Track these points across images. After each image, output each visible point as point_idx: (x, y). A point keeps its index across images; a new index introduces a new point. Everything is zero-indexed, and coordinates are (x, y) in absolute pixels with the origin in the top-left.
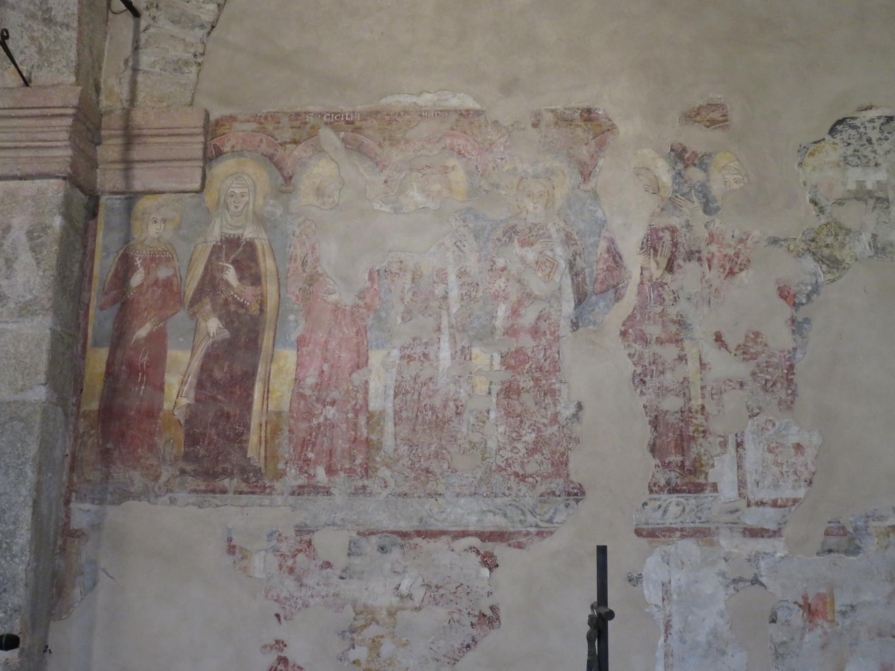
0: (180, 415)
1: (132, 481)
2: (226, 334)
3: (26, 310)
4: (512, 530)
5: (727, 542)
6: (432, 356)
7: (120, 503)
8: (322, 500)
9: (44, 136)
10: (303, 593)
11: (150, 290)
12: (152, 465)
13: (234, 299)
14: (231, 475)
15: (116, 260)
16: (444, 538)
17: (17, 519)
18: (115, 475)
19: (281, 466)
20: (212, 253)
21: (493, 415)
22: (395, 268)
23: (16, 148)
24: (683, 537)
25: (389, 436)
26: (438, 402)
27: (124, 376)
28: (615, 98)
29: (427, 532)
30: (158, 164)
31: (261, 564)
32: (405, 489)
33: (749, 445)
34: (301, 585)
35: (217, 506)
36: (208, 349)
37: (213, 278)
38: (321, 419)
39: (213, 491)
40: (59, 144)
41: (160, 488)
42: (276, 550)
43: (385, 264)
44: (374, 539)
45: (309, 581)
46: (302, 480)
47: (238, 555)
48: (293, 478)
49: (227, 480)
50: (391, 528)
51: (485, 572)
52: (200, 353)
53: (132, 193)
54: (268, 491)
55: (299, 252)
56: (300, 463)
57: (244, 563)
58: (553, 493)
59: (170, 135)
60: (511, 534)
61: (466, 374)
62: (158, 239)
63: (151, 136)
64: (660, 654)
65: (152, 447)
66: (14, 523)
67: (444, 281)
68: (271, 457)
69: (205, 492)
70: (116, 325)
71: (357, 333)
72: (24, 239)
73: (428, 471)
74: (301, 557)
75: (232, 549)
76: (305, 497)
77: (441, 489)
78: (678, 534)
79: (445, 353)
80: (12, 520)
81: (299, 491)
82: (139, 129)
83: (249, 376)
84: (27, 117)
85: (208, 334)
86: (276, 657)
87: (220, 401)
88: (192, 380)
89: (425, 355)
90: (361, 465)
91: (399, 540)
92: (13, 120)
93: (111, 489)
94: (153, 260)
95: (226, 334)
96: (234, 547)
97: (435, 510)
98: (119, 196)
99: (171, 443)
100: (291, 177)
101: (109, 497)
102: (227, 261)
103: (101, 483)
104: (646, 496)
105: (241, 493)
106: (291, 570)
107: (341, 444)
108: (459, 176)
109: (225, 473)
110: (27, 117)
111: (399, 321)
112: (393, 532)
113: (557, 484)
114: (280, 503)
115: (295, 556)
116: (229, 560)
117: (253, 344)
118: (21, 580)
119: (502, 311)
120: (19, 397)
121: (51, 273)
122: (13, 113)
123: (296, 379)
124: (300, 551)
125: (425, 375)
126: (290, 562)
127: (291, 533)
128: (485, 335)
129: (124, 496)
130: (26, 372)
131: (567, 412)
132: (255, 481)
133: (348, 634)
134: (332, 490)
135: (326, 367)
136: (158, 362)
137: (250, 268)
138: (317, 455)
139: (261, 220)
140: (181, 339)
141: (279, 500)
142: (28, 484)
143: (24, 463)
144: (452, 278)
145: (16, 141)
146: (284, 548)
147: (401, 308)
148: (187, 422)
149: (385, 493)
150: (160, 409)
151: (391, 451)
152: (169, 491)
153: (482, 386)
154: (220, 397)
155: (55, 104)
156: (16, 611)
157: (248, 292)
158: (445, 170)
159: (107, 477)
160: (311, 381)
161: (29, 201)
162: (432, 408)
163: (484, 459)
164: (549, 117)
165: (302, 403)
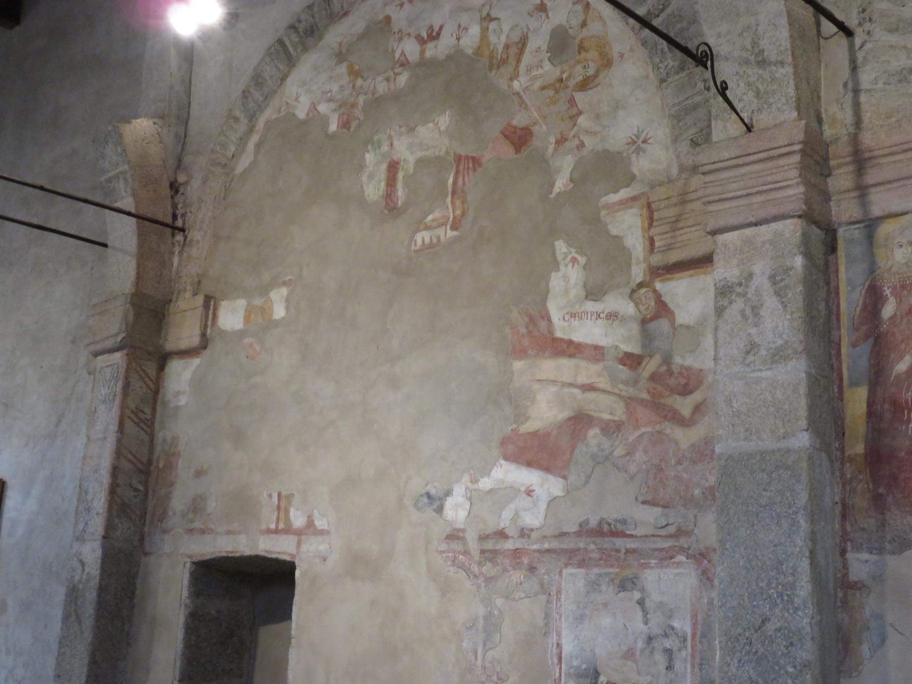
3: (778, 356)
9: (775, 178)
15: (863, 292)
23: (748, 195)
27: (888, 416)
30: (895, 185)
40: (790, 183)
53: (871, 219)
63: (884, 156)
66: (793, 574)
70: (872, 362)
93: (889, 537)
98: (857, 226)
103: (877, 531)
110: (755, 162)
118: (807, 633)
120: (783, 444)
121: (799, 314)
122: (740, 161)
156: (805, 666)
159: (883, 525)
161: (767, 246)
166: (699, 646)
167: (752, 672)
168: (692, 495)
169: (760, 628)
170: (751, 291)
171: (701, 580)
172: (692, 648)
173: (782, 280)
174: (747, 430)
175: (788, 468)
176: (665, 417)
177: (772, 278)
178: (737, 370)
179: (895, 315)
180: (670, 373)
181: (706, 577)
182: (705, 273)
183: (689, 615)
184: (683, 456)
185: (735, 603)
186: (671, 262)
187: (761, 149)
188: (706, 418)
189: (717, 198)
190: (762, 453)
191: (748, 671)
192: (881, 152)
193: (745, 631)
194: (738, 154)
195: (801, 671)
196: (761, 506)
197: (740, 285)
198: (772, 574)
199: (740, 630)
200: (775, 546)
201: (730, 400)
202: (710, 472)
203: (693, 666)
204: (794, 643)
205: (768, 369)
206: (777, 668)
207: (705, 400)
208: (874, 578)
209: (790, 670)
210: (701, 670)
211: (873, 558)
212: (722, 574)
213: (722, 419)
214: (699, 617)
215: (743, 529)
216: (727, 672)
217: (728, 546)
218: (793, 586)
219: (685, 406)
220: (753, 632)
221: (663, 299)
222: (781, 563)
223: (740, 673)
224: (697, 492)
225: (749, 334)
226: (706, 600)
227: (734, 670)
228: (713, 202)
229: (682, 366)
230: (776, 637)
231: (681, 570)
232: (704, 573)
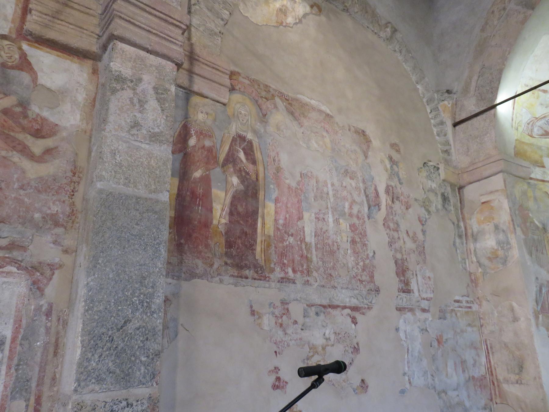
0: (222, 229)
1: (197, 266)
2: (242, 187)
3: (154, 138)
4: (360, 306)
5: (418, 313)
6: (326, 219)
7: (189, 280)
8: (292, 286)
9: (170, 33)
10: (287, 338)
11: (200, 151)
12: (209, 257)
13: (244, 169)
14: (249, 268)
15: (180, 126)
16: (339, 309)
17: (155, 284)
18: (186, 261)
19: (272, 266)
20: (233, 140)
21: (349, 252)
22: (309, 174)
23: (149, 31)
24: (408, 311)
25: (314, 256)
26: (330, 242)
27: (188, 199)
28: (371, 130)
29: (332, 305)
30: (206, 80)
31: (267, 322)
32: (323, 283)
33: (418, 276)
34: (286, 334)
35: (244, 286)
36: (234, 193)
37: (233, 155)
38: (288, 243)
39: (241, 277)
40: (177, 42)
41: (213, 272)
42: (273, 313)
43: (306, 171)
44: (313, 308)
45: (289, 331)
46: (282, 275)
47: (256, 316)
48: (278, 274)
49: (247, 271)
50: (319, 303)
51: (353, 325)
52: (230, 195)
53: (190, 90)
54: (267, 279)
55: (273, 154)
56: (281, 265)
57: (259, 321)
58: (371, 290)
59: (213, 68)
60: (360, 308)
61: (339, 232)
62: (204, 123)
63: (203, 63)
64: (406, 362)
65: (207, 246)
66: (153, 287)
67: (327, 186)
68: (268, 260)
69: (237, 277)
70: (182, 166)
71: (298, 202)
72: (151, 92)
73: (331, 275)
74: (284, 317)
75: (253, 313)
76: (284, 284)
77: (336, 285)
78: (407, 310)
79: (331, 220)
80: (151, 285)
81: (282, 280)
82: (198, 57)
83: (255, 213)
84: (155, 16)
85: (233, 185)
86: (275, 377)
87: (242, 224)
88: (227, 209)
89: (324, 219)
90: (306, 269)
91: (323, 309)
92: (145, 13)
93: (184, 269)
94: (201, 134)
95: (242, 187)
96: (254, 311)
97: (335, 295)
98: (181, 90)
99: (218, 244)
100: (265, 115)
101: (183, 275)
102: (240, 147)
103: (178, 265)
104: (397, 293)
105: (255, 279)
106: (281, 325)
107: (297, 258)
108: (327, 140)
109: (248, 267)
110: (155, 16)
111: (313, 200)
112: (320, 305)
113: (371, 286)
114: (273, 287)
115: (282, 317)
116: (252, 319)
117: (255, 195)
118: (159, 330)
119: (347, 205)
120: (153, 196)
121: (172, 119)
122: (148, 9)
123: (275, 220)
124: (284, 314)
125: (325, 228)
126: (280, 321)
127: (278, 304)
128: (343, 214)
129: (192, 275)
130: (157, 180)
131: (371, 254)
132: (261, 273)
133: (306, 361)
134: (296, 281)
135: (287, 216)
136: (207, 194)
137: (250, 155)
138: (288, 261)
139: (255, 132)
140: (219, 184)
141: (273, 284)
142: (162, 259)
143: (159, 244)
144: (329, 186)
145: (150, 27)
146: (277, 313)
147: (313, 195)
148: (226, 233)
149: (316, 284)
150: (211, 223)
151: (316, 263)
152: (219, 274)
153: (345, 239)
154: (241, 222)
155: (176, 17)
156: (156, 355)
157: (250, 168)
158: (323, 137)
159: (181, 262)
160: (281, 222)
161: (154, 69)
162: (329, 245)
163: (349, 272)
164: (353, 129)
165: (279, 233)
166: (19, 348)
167: (110, 364)
168: (32, 217)
169: (122, 327)
170: (139, 89)
171: (31, 290)
172: (10, 350)
173: (162, 94)
174: (126, 179)
175: (156, 213)
176: (14, 147)
177: (155, 89)
178: (123, 135)
179: (195, 146)
180: (26, 117)
181: (37, 288)
182: (71, 61)
183: (12, 321)
184: (29, 183)
185: (101, 308)
186: (47, 37)
187: (163, 12)
188: (57, 161)
189: (128, 19)
190: (137, 198)
191: (108, 364)
192: (203, 61)
193: (109, 330)
194: (148, 3)
195: (153, 359)
196: (132, 235)
197: (132, 81)
198: (137, 286)
199: (104, 330)
200: (141, 265)
201: (115, 154)
202: (54, 203)
203: (9, 367)
204: (149, 338)
205: (147, 144)
206: (133, 359)
207: (56, 148)
208: (173, 294)
209: (143, 359)
210: (16, 370)
211: (174, 282)
212: (92, 283)
213: (107, 165)
214: (24, 322)
215: (116, 250)
216: (86, 367)
217: (100, 261)
218: (151, 296)
219: (37, 146)
220: (115, 331)
221: (28, 58)
222: (144, 278)
223: (99, 366)
224: (37, 216)
225: (135, 116)
226: (33, 307)
227: (94, 364)
228: (123, 19)
229: (38, 115)
230: (135, 334)
231: (10, 279)
232: (34, 283)
